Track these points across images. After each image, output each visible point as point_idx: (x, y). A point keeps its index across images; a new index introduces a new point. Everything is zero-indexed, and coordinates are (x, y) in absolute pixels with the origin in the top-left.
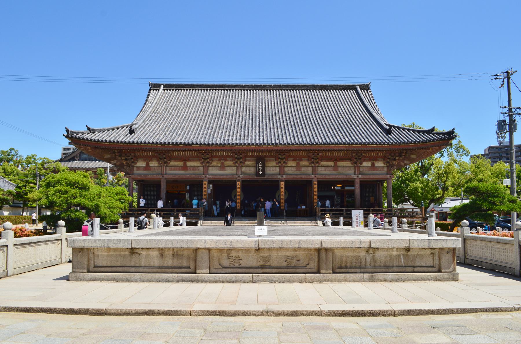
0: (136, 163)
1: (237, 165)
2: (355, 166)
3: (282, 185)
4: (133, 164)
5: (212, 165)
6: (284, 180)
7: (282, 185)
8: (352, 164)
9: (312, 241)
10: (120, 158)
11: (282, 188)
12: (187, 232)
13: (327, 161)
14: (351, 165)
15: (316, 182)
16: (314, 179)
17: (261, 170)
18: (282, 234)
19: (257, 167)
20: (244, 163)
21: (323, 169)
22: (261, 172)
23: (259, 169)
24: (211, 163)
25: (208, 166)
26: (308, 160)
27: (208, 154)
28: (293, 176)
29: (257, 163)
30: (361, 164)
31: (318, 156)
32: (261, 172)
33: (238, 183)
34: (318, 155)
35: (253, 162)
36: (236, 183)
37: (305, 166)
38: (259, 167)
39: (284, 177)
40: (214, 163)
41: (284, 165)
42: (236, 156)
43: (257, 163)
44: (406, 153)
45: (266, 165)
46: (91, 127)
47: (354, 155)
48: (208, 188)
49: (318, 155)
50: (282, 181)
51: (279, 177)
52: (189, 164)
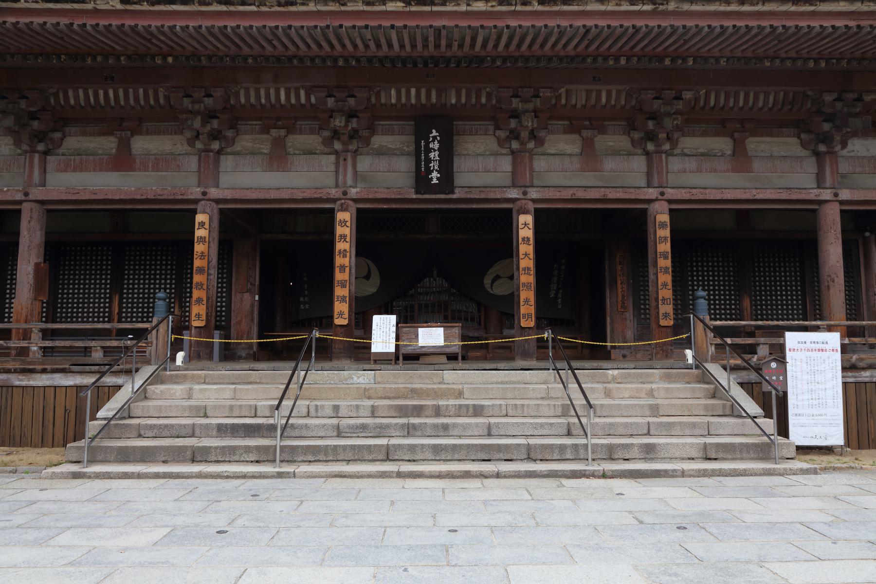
1: (337, 146)
2: (817, 154)
3: (525, 227)
5: (238, 147)
6: (531, 206)
7: (525, 227)
8: (804, 145)
9: (172, 426)
11: (526, 240)
12: (807, 469)
13: (705, 134)
14: (800, 151)
15: (665, 218)
16: (656, 206)
17: (434, 165)
18: (375, 435)
19: (420, 155)
21: (691, 164)
22: (435, 175)
23: (428, 161)
24: (233, 141)
25: (219, 152)
26: (631, 127)
27: (209, 95)
28: (572, 191)
29: (421, 135)
30: (844, 145)
31: (680, 105)
32: (435, 175)
33: (341, 216)
34: (679, 98)
35: (404, 138)
36: (333, 218)
37: (615, 153)
38: (428, 150)
39: (534, 194)
40: (245, 142)
41: (531, 145)
42: (331, 102)
43: (421, 135)
45: (458, 149)
48: (160, 163)
49: (679, 98)
50: (526, 212)
51: (513, 194)
52: (141, 145)
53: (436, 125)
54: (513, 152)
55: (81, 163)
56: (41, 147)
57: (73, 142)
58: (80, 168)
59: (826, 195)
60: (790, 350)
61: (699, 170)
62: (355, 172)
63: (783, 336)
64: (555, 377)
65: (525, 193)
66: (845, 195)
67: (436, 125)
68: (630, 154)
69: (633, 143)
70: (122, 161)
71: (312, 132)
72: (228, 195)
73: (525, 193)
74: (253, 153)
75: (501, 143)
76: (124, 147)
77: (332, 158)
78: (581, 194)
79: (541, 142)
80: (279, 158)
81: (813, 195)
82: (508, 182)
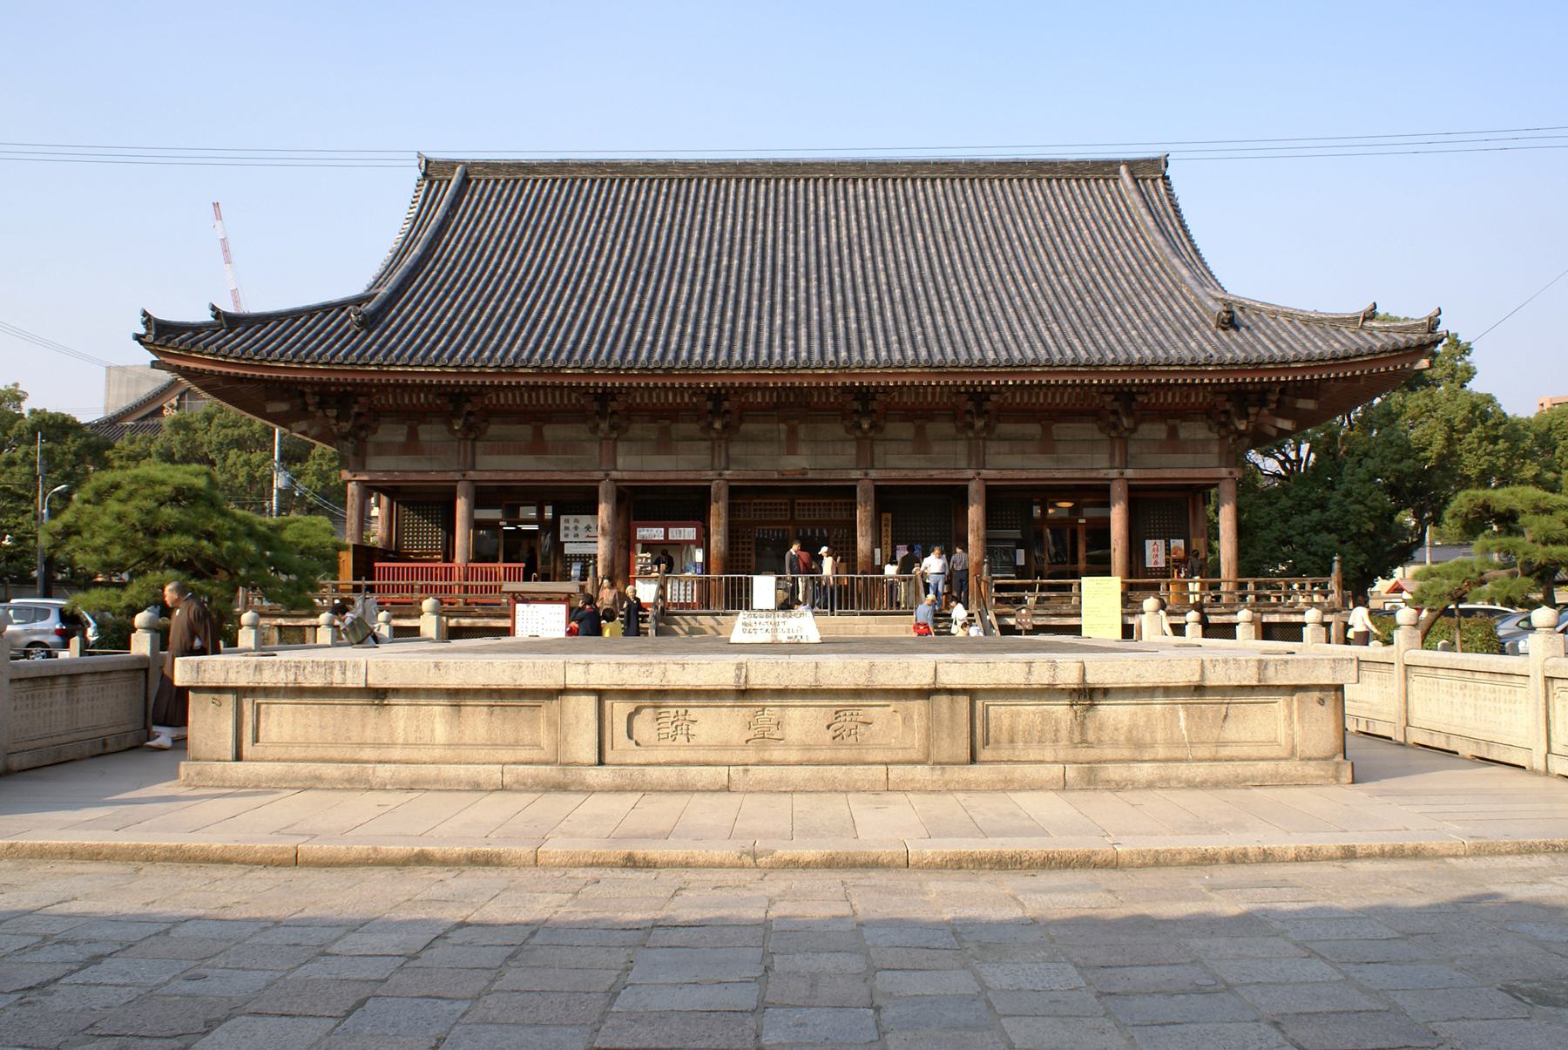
0: (375, 431)
4: (363, 434)
8: (1101, 430)
10: (320, 413)
14: (1098, 436)
20: (737, 429)
21: (1004, 447)
24: (627, 430)
28: (904, 472)
44: (1282, 392)
46: (228, 307)
47: (1108, 398)
52: (549, 431)
53: (198, 538)
54: (857, 439)
55: (503, 447)
56: (472, 436)
57: (494, 429)
59: (1114, 473)
60: (1030, 664)
61: (1011, 453)
62: (727, 456)
63: (511, 615)
64: (888, 747)
66: (1129, 473)
67: (198, 538)
68: (955, 439)
69: (958, 430)
70: (537, 446)
71: (692, 422)
72: (626, 476)
74: (643, 440)
75: (848, 430)
76: (538, 433)
77: (708, 443)
78: (911, 474)
79: (882, 429)
80: (664, 445)
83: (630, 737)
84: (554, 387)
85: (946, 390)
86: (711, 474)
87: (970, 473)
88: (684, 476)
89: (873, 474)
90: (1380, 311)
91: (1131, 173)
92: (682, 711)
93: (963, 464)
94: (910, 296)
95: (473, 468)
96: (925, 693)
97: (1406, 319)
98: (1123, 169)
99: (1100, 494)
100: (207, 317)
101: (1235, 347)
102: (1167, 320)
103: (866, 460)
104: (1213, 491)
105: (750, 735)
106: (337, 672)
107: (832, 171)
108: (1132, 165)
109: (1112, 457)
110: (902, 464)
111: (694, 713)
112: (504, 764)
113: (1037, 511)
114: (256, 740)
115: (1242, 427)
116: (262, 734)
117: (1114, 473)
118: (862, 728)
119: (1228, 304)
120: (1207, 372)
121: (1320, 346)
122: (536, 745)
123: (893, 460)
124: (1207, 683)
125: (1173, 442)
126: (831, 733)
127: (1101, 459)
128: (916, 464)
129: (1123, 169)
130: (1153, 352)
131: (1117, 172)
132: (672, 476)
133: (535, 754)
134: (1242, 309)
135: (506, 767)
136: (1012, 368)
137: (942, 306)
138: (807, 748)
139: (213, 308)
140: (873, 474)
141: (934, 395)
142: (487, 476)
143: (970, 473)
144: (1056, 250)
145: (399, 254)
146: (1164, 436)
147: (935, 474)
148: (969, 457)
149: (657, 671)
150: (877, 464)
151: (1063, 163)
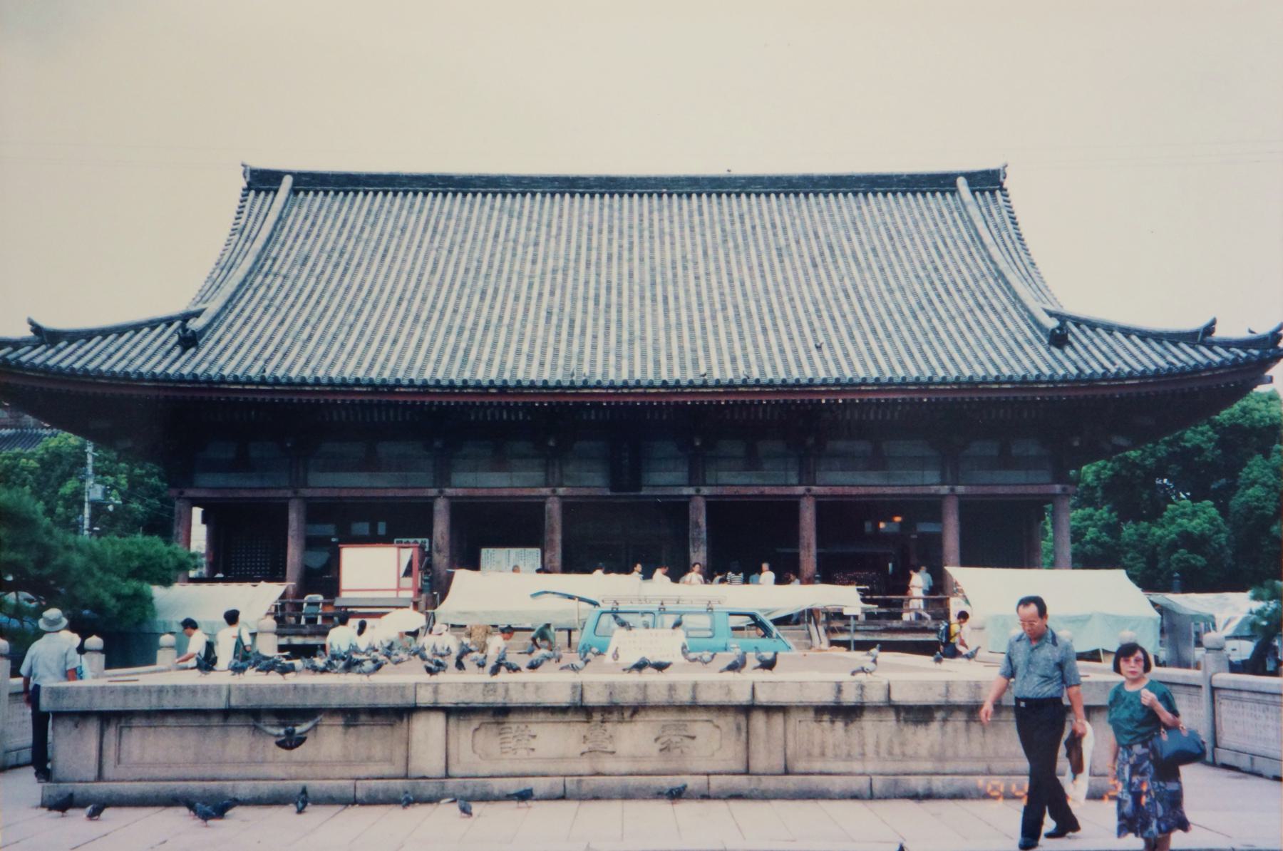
28: (735, 489)
46: (50, 322)
52: (386, 449)
55: (336, 465)
58: (336, 468)
59: (945, 490)
65: (698, 491)
66: (960, 489)
73: (698, 491)
78: (743, 491)
80: (500, 463)
81: (933, 490)
82: (685, 481)
83: (474, 752)
84: (389, 404)
85: (769, 409)
86: (545, 491)
87: (800, 490)
88: (518, 493)
89: (705, 491)
90: (1220, 333)
91: (970, 184)
92: (522, 727)
93: (794, 480)
94: (743, 314)
95: (306, 486)
96: (747, 710)
97: (1203, 337)
98: (961, 182)
99: (932, 508)
100: (27, 332)
101: (1063, 364)
102: (692, 329)
103: (807, 477)
104: (1049, 506)
105: (585, 748)
106: (154, 696)
107: (665, 186)
108: (972, 178)
109: (943, 476)
110: (734, 482)
111: (534, 729)
112: (358, 779)
113: (868, 526)
114: (119, 761)
115: (1076, 444)
116: (123, 756)
117: (945, 490)
118: (687, 741)
119: (1062, 318)
120: (1038, 389)
121: (1151, 359)
122: (390, 760)
123: (725, 477)
124: (757, 703)
125: (1006, 461)
126: (658, 746)
127: (932, 476)
128: (747, 481)
129: (961, 182)
130: (986, 370)
131: (954, 184)
132: (505, 493)
133: (387, 770)
134: (1077, 325)
135: (359, 783)
136: (842, 386)
137: (775, 325)
138: (634, 758)
139: (31, 323)
140: (705, 491)
141: (764, 412)
142: (318, 493)
143: (800, 490)
144: (408, 248)
145: (226, 267)
146: (995, 453)
147: (767, 490)
148: (800, 475)
149: (501, 691)
150: (708, 481)
151: (898, 176)
